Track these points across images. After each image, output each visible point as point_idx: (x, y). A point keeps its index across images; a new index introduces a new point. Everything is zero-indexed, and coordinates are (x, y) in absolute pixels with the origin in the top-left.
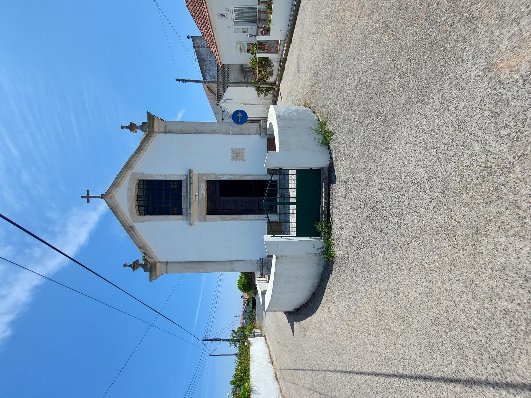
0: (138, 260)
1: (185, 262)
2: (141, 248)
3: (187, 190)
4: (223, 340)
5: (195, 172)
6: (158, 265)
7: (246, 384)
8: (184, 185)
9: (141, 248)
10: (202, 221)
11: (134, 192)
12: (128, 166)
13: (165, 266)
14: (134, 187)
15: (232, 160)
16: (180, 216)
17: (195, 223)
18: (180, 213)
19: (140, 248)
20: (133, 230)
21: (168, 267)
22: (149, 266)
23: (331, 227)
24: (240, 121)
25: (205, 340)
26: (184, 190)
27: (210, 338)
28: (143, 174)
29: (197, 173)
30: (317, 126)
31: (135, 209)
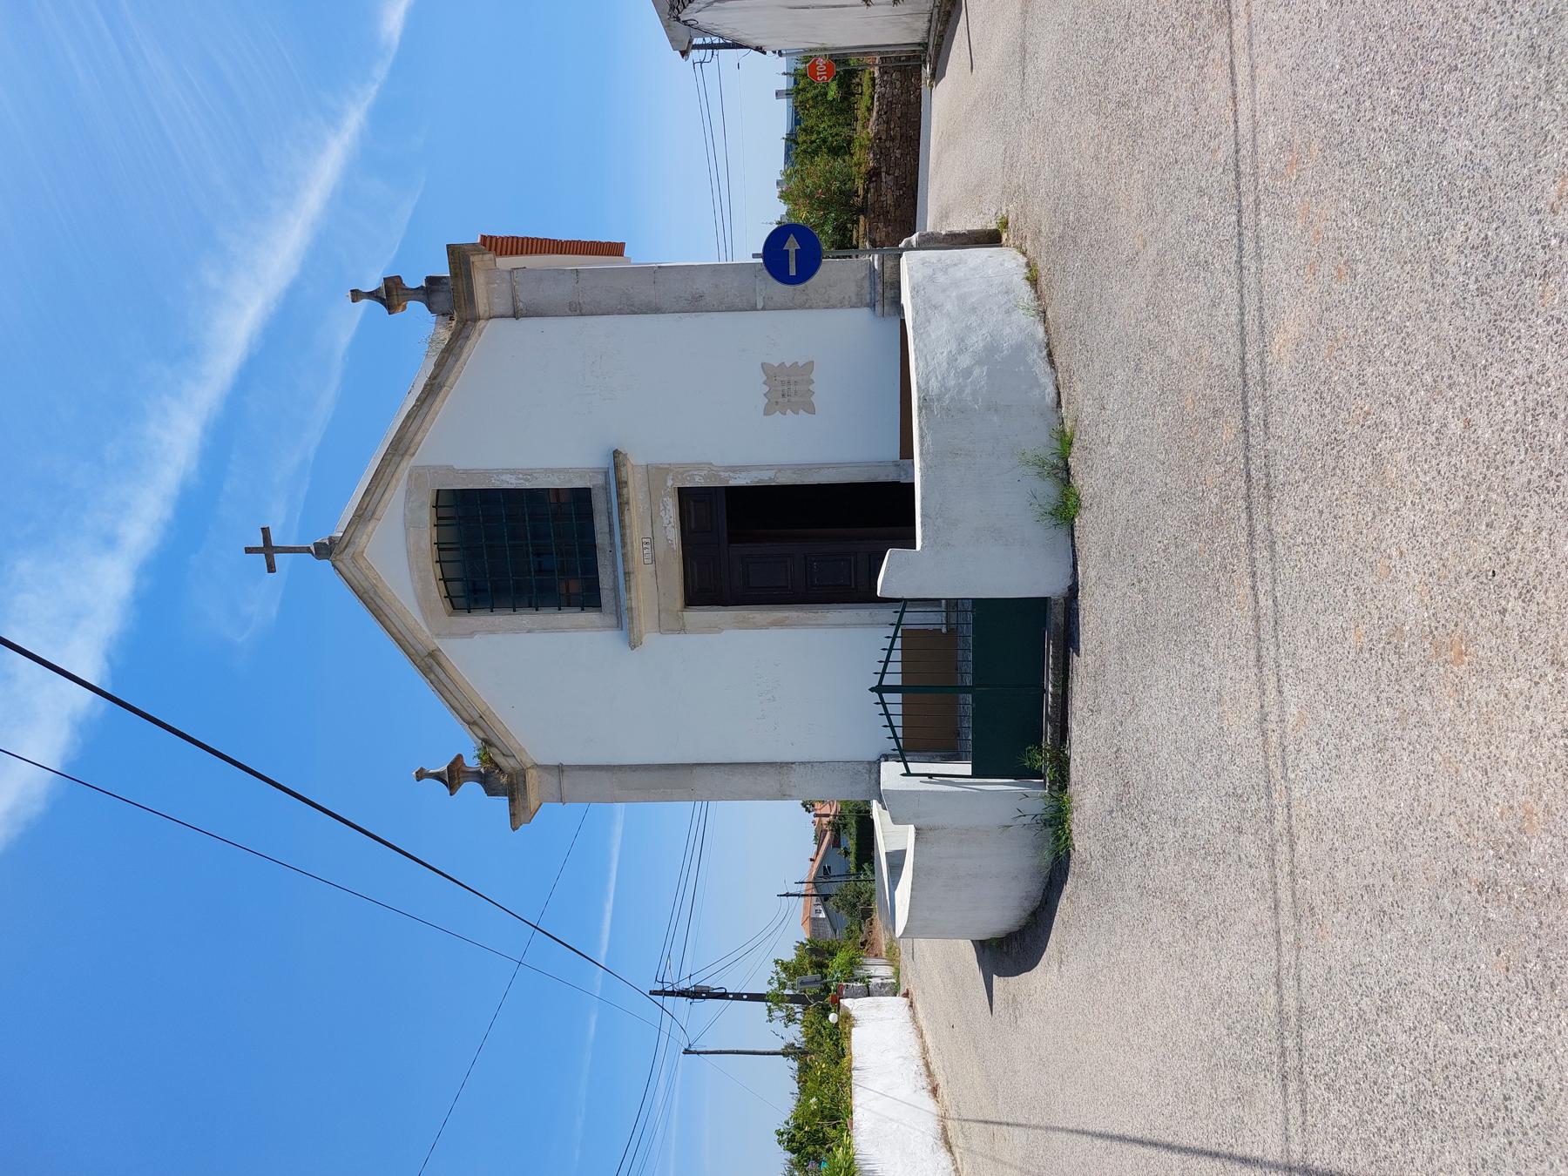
0: (459, 757)
1: (621, 767)
2: (474, 723)
3: (611, 525)
4: (738, 997)
5: (636, 459)
6: (532, 777)
7: (840, 1153)
8: (598, 504)
9: (474, 723)
10: (673, 631)
11: (426, 536)
12: (399, 447)
13: (555, 781)
14: (427, 516)
15: (767, 412)
16: (590, 617)
17: (646, 638)
18: (589, 598)
19: (471, 723)
20: (439, 664)
21: (565, 783)
22: (500, 777)
23: (1067, 763)
24: (793, 272)
25: (664, 993)
26: (600, 523)
27: (685, 985)
28: (450, 469)
29: (642, 462)
30: (1040, 443)
31: (436, 591)
